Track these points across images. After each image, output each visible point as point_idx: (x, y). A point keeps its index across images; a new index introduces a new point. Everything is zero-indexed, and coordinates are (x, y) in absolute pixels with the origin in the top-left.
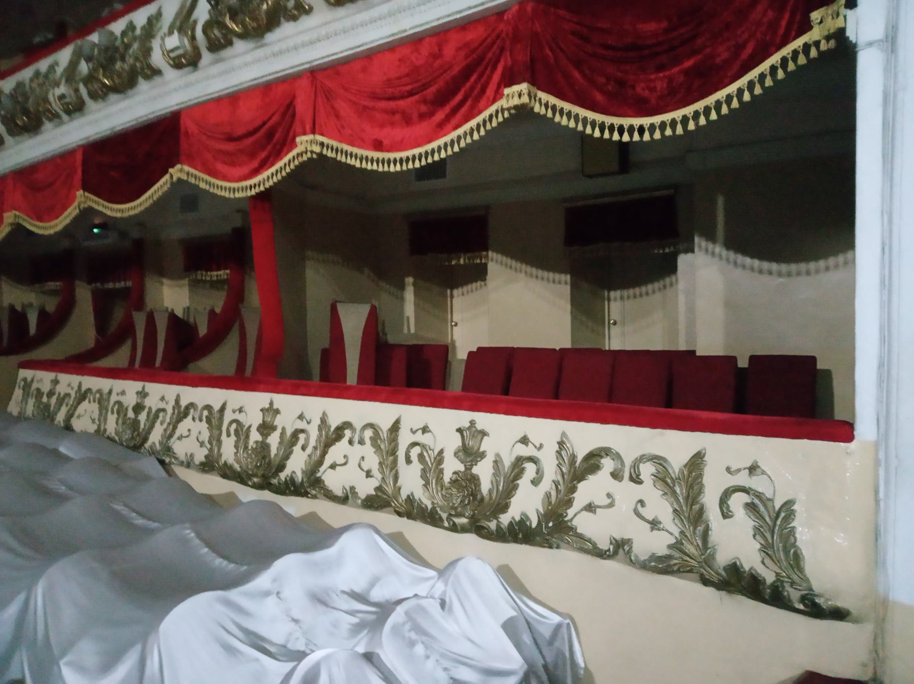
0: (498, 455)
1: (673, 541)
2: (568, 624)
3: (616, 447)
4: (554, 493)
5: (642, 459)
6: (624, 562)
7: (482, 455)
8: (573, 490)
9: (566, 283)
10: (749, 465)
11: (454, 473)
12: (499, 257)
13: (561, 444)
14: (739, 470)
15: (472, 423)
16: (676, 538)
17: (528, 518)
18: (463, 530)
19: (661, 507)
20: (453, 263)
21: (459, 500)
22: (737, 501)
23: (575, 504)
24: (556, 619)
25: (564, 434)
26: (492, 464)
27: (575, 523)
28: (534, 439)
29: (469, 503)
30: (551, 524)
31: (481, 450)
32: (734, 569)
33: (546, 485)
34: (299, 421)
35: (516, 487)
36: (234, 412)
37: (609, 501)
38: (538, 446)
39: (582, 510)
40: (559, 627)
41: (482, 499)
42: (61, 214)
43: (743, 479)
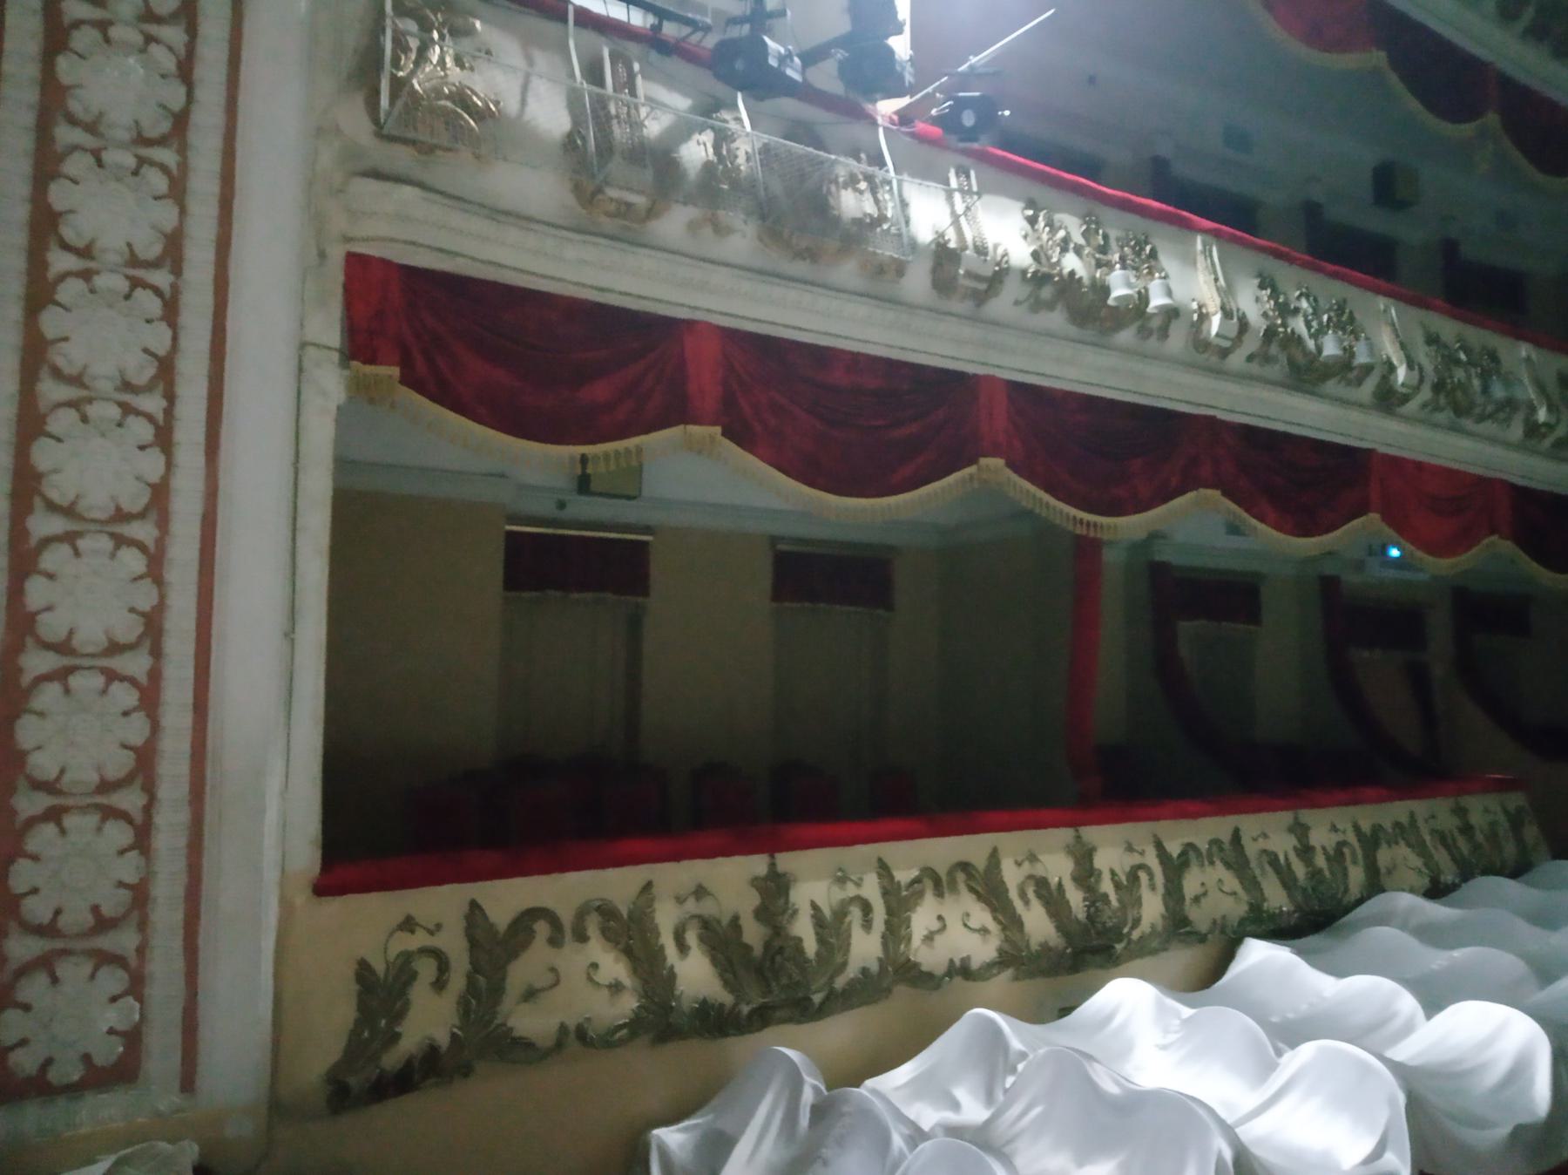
3: (548, 903)
22: (691, 938)
28: (420, 915)
34: (405, 935)
36: (1255, 840)
42: (1206, 417)
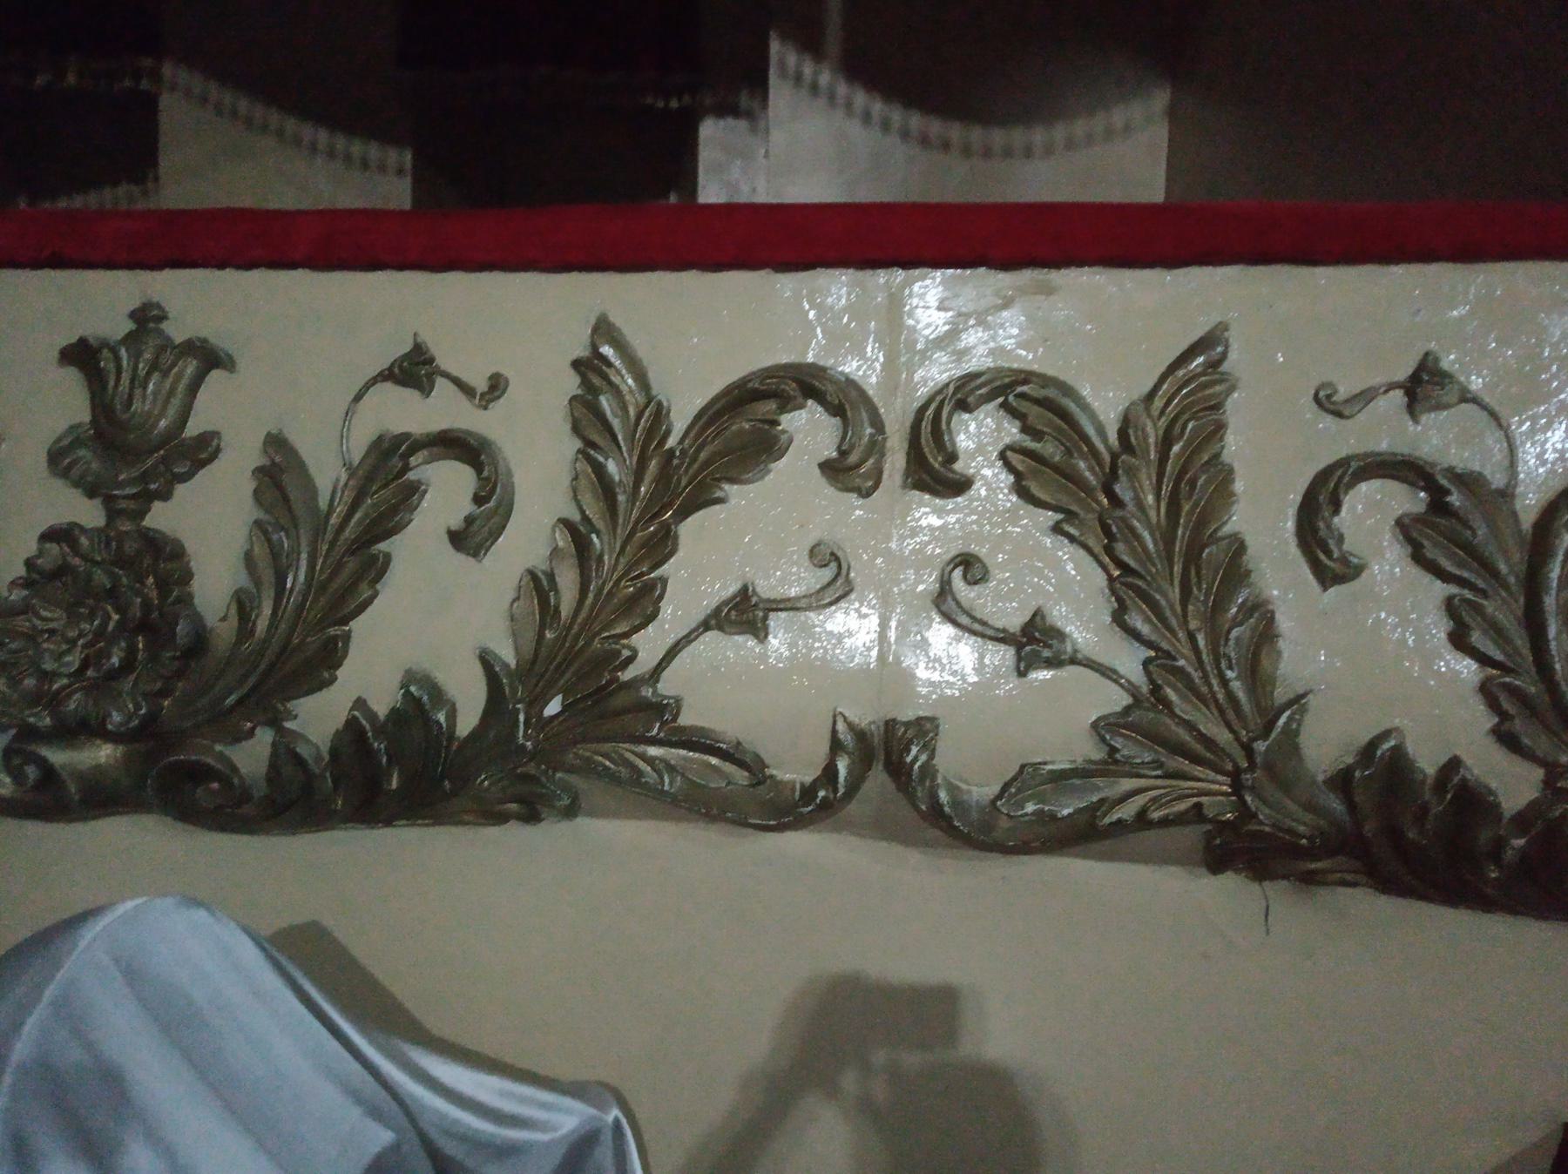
0: (276, 443)
1: (1118, 700)
2: (617, 1125)
4: (567, 580)
5: (964, 394)
6: (882, 829)
7: (204, 451)
8: (662, 546)
9: (400, 172)
10: (1403, 373)
11: (49, 536)
12: (197, 83)
13: (589, 368)
14: (1366, 397)
15: (147, 317)
16: (1132, 689)
17: (437, 694)
18: (99, 798)
19: (1062, 580)
20: (40, 81)
21: (73, 660)
23: (667, 610)
24: (567, 1118)
25: (604, 329)
26: (249, 486)
27: (667, 686)
29: (128, 665)
30: (553, 707)
31: (192, 429)
32: (1382, 770)
33: (529, 538)
35: (376, 569)
37: (827, 574)
38: (481, 385)
39: (706, 626)
40: (582, 1147)
41: (200, 642)
43: (1385, 428)
